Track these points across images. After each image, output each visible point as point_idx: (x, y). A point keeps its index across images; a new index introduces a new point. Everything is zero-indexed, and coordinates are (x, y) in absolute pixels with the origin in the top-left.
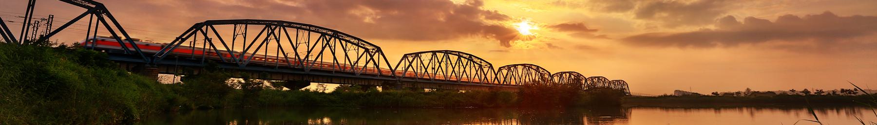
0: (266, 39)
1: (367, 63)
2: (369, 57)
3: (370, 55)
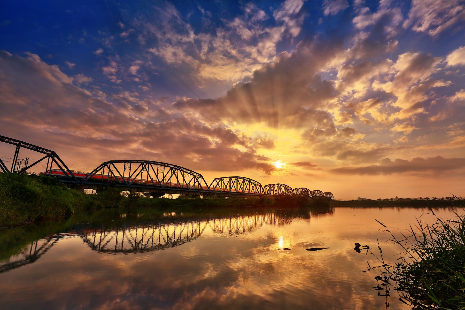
0: (141, 171)
1: (195, 183)
2: (196, 180)
3: (197, 179)
